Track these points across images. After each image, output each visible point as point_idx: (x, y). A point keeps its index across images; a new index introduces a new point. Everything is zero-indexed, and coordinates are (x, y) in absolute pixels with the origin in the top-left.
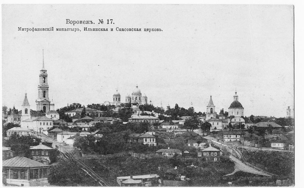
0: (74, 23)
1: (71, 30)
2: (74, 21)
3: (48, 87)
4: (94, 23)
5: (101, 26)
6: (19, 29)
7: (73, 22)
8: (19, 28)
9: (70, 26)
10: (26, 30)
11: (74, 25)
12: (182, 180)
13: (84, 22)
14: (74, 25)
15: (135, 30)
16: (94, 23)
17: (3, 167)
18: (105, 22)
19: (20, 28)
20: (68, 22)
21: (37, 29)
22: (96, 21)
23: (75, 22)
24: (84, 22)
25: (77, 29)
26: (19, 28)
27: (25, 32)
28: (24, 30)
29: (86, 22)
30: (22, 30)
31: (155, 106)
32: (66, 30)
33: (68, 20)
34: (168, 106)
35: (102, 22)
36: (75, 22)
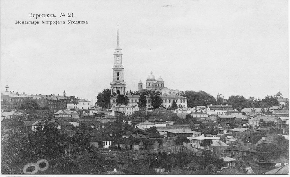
0: (37, 16)
1: (31, 23)
2: (37, 15)
3: (123, 68)
4: (56, 17)
5: (62, 19)
6: (17, 22)
7: (36, 15)
8: (16, 21)
9: (33, 19)
10: (50, 23)
11: (37, 18)
12: (201, 143)
13: (47, 15)
14: (37, 18)
15: (84, 23)
16: (56, 17)
17: (288, 116)
18: (67, 15)
19: (17, 21)
20: (31, 16)
21: (60, 22)
22: (58, 15)
23: (37, 16)
24: (47, 15)
25: (37, 22)
26: (16, 21)
27: (48, 24)
28: (48, 23)
29: (48, 16)
30: (45, 23)
31: (214, 93)
32: (27, 23)
33: (31, 14)
34: (7, 87)
35: (63, 16)
36: (37, 16)
